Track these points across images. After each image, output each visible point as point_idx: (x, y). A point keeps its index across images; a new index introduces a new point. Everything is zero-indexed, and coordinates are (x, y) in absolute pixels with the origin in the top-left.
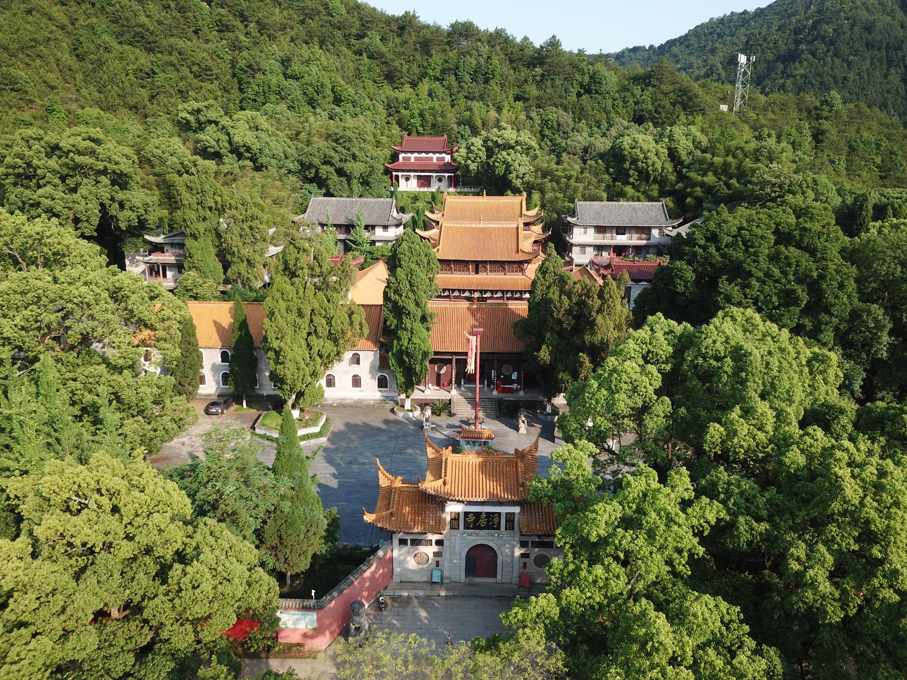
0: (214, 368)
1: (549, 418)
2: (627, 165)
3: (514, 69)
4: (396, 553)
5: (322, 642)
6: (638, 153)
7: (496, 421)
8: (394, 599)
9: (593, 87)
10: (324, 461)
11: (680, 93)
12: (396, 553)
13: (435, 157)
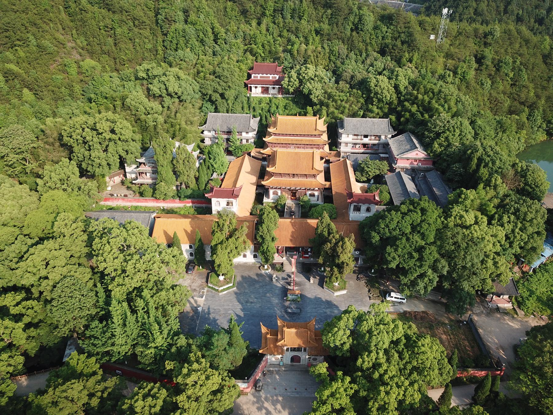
0: (187, 251)
1: (322, 273)
2: (372, 95)
3: (316, 9)
4: (268, 357)
5: (248, 390)
6: (379, 90)
7: (301, 275)
8: (268, 371)
9: (360, 27)
10: (236, 301)
11: (408, 35)
12: (268, 357)
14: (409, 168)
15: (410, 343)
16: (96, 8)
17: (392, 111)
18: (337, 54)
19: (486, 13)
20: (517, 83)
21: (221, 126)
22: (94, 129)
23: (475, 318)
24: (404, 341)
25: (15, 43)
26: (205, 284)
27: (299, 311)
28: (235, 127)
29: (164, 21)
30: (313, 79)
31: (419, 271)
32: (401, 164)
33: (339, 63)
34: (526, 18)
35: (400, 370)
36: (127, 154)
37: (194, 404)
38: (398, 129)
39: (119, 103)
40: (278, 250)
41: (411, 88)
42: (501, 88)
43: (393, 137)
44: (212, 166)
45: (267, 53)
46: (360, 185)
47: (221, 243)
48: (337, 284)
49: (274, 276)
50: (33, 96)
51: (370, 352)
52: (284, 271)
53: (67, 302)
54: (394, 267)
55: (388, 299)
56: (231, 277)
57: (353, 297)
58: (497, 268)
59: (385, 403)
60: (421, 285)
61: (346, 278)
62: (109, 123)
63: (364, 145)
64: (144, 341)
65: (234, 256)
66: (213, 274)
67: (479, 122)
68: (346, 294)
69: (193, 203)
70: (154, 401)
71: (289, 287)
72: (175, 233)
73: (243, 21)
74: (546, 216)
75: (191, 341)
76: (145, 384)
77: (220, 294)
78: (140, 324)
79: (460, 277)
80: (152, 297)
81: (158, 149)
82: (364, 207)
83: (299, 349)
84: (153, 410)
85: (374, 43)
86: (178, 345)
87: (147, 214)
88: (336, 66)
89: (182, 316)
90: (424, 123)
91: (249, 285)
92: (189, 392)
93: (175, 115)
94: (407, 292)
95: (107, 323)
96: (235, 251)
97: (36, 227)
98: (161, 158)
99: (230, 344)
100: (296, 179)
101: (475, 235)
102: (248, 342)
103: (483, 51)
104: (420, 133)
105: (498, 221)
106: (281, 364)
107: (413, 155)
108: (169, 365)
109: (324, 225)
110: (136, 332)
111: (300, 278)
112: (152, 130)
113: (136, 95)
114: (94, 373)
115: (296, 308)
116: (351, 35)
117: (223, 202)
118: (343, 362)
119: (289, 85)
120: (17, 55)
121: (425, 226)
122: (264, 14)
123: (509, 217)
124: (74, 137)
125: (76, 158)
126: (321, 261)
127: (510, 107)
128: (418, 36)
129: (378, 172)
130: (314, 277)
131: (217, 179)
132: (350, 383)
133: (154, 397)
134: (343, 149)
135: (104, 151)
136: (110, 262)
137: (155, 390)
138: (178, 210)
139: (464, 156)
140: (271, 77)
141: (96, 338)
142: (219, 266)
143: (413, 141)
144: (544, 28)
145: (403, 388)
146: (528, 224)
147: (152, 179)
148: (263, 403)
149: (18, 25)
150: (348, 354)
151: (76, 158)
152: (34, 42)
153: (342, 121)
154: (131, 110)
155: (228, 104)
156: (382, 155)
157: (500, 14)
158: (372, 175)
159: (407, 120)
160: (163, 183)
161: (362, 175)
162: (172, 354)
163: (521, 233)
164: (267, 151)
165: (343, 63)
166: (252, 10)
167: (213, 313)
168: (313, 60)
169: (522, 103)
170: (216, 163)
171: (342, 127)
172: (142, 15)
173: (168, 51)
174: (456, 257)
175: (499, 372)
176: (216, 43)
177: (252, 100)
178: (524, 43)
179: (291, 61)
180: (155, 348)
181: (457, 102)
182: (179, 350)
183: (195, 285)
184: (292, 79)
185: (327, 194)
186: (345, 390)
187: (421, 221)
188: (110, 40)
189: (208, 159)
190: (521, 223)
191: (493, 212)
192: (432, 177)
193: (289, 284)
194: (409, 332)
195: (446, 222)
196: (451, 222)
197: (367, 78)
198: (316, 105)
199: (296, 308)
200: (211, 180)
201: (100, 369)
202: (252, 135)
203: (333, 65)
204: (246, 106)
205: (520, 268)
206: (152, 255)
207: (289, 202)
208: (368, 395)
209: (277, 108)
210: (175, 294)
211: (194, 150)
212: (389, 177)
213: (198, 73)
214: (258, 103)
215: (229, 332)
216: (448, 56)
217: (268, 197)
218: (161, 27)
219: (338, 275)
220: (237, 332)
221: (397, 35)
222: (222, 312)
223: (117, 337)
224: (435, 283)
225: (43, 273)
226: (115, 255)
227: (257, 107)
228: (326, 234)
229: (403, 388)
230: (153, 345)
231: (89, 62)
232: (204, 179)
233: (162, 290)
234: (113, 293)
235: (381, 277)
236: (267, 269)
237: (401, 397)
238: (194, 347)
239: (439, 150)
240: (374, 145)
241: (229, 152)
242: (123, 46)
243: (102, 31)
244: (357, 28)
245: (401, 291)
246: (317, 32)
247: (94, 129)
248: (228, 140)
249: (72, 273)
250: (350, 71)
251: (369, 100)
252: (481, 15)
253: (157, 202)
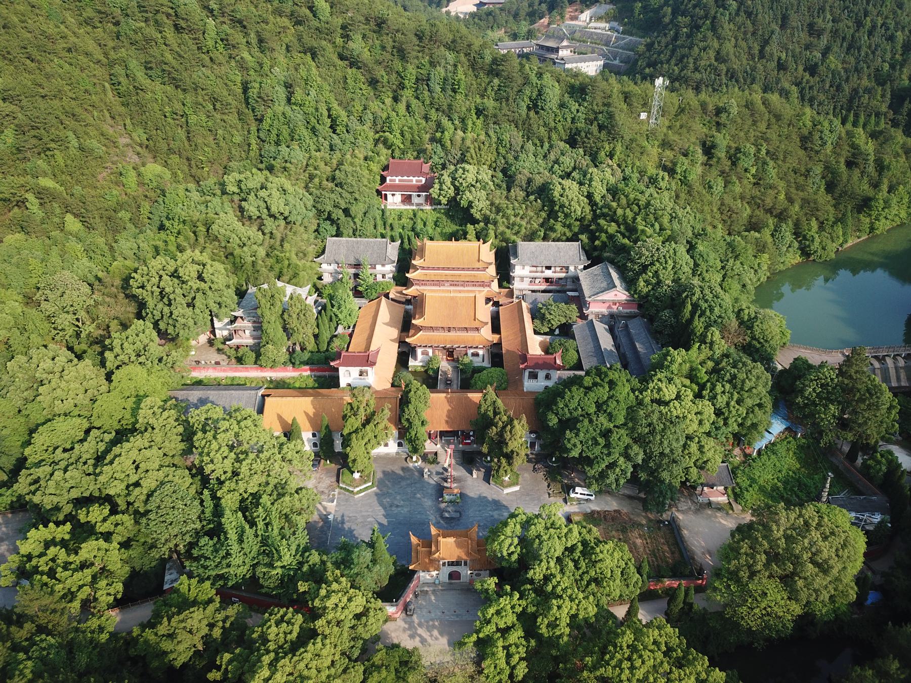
0: (309, 440)
2: (557, 208)
13: (414, 179)
14: (606, 313)
15: (587, 550)
16: (158, 87)
17: (584, 229)
18: (508, 145)
19: (733, 58)
20: (761, 182)
21: (346, 257)
22: (175, 275)
23: (680, 516)
24: (580, 548)
25: (48, 146)
26: (335, 484)
27: (458, 515)
28: (365, 259)
29: (257, 101)
30: (472, 186)
31: (608, 460)
32: (597, 307)
33: (510, 157)
34: (792, 65)
35: (576, 581)
36: (220, 307)
37: (336, 629)
38: (593, 257)
39: (202, 229)
40: (430, 435)
41: (611, 197)
42: (738, 189)
43: (585, 268)
44: (336, 316)
45: (408, 144)
46: (539, 338)
47: (356, 431)
48: (507, 479)
49: (426, 470)
50: (80, 224)
51: (541, 561)
52: (438, 463)
53: (168, 514)
54: (577, 456)
55: (572, 495)
56: (370, 474)
57: (528, 495)
58: (702, 452)
59: (556, 619)
60: (612, 477)
61: (518, 470)
62: (196, 267)
63: (547, 280)
64: (267, 560)
65: (373, 447)
66: (345, 470)
67: (700, 248)
68: (518, 491)
69: (311, 370)
70: (290, 627)
71: (445, 484)
72: (294, 419)
73: (372, 94)
74: (770, 383)
75: (325, 558)
76: (276, 609)
77: (356, 496)
78: (260, 538)
79: (659, 466)
80: (272, 504)
81: (263, 301)
82: (542, 374)
83: (458, 563)
84: (289, 637)
85: (560, 128)
86: (310, 563)
87: (253, 392)
88: (507, 163)
89: (309, 527)
90: (624, 249)
91: (394, 482)
92: (330, 617)
93: (282, 246)
94: (595, 487)
95: (219, 539)
96: (373, 441)
97: (111, 417)
98: (267, 313)
99: (374, 561)
100: (452, 334)
101: (675, 413)
102: (394, 556)
103: (713, 136)
104: (620, 264)
105: (711, 391)
106: (437, 582)
107: (610, 296)
108: (302, 587)
109: (488, 403)
110: (255, 549)
111: (460, 472)
112: (250, 267)
113: (227, 221)
114: (211, 601)
115: (455, 511)
116: (528, 115)
117: (355, 371)
118: (512, 575)
119: (440, 194)
120: (53, 163)
121: (612, 404)
122: (402, 86)
123: (723, 386)
124: (149, 288)
125: (150, 315)
126: (485, 449)
127: (751, 217)
128: (622, 118)
129: (563, 321)
130: (478, 470)
131: (343, 334)
132: (518, 599)
133: (288, 623)
134: (517, 285)
135: (188, 305)
136: (219, 465)
137: (290, 615)
138: (292, 382)
139: (676, 298)
140: (415, 180)
141: (206, 558)
142: (354, 461)
143: (610, 274)
144: (818, 79)
145: (577, 601)
146: (746, 395)
147: (254, 339)
148: (416, 629)
149: (52, 120)
150: (516, 565)
151: (150, 315)
152: (74, 143)
153: (515, 247)
154: (219, 241)
155: (355, 223)
156: (570, 293)
157: (753, 59)
158: (555, 324)
160: (270, 346)
161: (543, 326)
162: (303, 574)
163: (737, 407)
164: (411, 291)
165: (516, 158)
166: (385, 80)
167: (348, 521)
168: (474, 155)
169: (769, 211)
170: (341, 312)
171: (516, 255)
172: (225, 93)
173: (267, 146)
174: (650, 442)
175: (700, 582)
176: (334, 132)
177: (388, 214)
178: (773, 120)
179: (442, 154)
180: (282, 567)
181: (672, 218)
182: (312, 568)
183: (323, 486)
184: (444, 187)
185: (495, 351)
186: (513, 607)
187: (608, 398)
188: (182, 133)
189: (329, 306)
190: (738, 393)
191: (705, 379)
192: (636, 328)
193: (445, 480)
194: (588, 537)
195: (641, 396)
196: (647, 396)
197: (550, 183)
198: (478, 222)
199: (455, 511)
200: (336, 336)
201: (216, 595)
202: (389, 269)
203: (503, 161)
204: (380, 223)
205: (743, 450)
206: (271, 452)
207: (445, 365)
208: (537, 611)
209: (425, 225)
210: (300, 500)
211: (310, 294)
212: (578, 327)
213: (311, 177)
214: (396, 218)
215: (371, 545)
216: (665, 144)
217: (416, 359)
218: (253, 111)
219: (507, 467)
220: (382, 545)
221: (592, 117)
222: (359, 520)
223: (234, 556)
224: (629, 475)
225: (133, 479)
226: (225, 454)
227: (396, 224)
228: (491, 414)
229: (577, 601)
230: (279, 564)
231: (153, 169)
232: (326, 336)
233: (283, 495)
234: (223, 501)
235: (565, 467)
236: (416, 462)
237: (573, 612)
238: (329, 565)
239: (645, 290)
240: (560, 279)
241: (358, 294)
242: (200, 141)
243: (169, 119)
244: (535, 106)
245: (588, 486)
246: (479, 112)
247: (175, 275)
248: (356, 276)
249: (170, 478)
250: (526, 171)
251: (552, 214)
252: (724, 61)
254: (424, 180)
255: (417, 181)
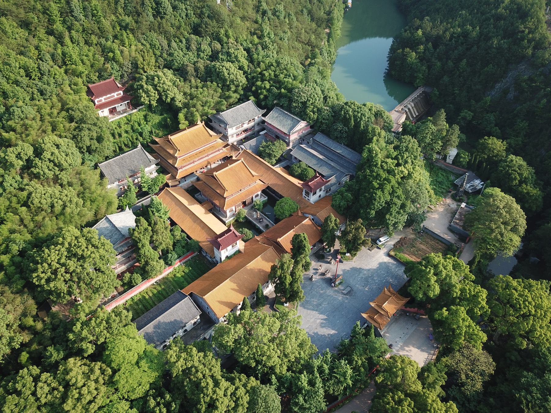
2: (228, 83)
63: (245, 131)
159: (266, 97)
239: (316, 117)
244: (158, 13)
253: (149, 282)
254: (122, 92)
255: (117, 95)
